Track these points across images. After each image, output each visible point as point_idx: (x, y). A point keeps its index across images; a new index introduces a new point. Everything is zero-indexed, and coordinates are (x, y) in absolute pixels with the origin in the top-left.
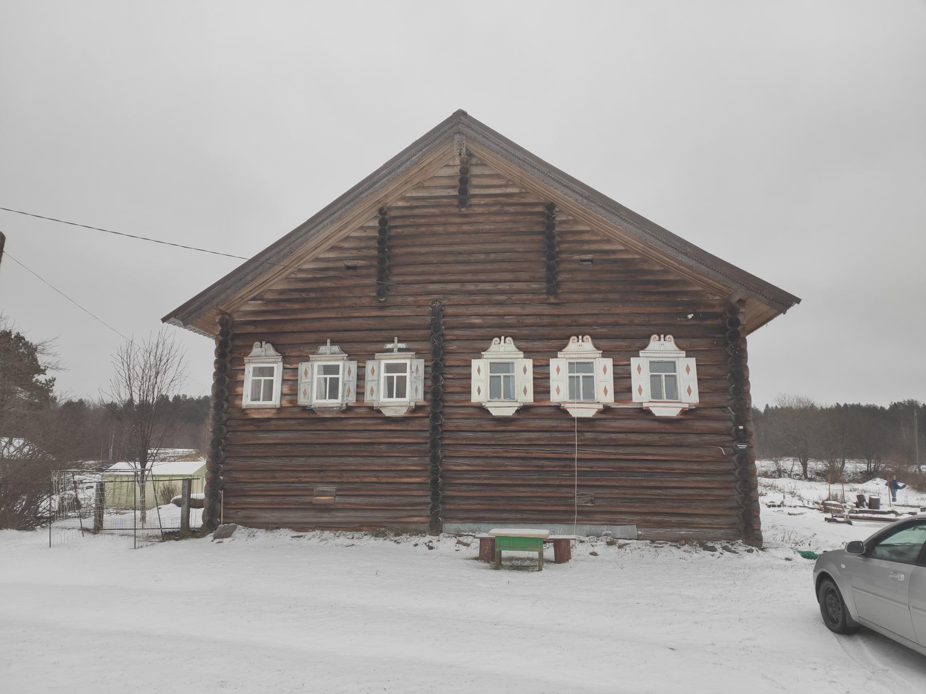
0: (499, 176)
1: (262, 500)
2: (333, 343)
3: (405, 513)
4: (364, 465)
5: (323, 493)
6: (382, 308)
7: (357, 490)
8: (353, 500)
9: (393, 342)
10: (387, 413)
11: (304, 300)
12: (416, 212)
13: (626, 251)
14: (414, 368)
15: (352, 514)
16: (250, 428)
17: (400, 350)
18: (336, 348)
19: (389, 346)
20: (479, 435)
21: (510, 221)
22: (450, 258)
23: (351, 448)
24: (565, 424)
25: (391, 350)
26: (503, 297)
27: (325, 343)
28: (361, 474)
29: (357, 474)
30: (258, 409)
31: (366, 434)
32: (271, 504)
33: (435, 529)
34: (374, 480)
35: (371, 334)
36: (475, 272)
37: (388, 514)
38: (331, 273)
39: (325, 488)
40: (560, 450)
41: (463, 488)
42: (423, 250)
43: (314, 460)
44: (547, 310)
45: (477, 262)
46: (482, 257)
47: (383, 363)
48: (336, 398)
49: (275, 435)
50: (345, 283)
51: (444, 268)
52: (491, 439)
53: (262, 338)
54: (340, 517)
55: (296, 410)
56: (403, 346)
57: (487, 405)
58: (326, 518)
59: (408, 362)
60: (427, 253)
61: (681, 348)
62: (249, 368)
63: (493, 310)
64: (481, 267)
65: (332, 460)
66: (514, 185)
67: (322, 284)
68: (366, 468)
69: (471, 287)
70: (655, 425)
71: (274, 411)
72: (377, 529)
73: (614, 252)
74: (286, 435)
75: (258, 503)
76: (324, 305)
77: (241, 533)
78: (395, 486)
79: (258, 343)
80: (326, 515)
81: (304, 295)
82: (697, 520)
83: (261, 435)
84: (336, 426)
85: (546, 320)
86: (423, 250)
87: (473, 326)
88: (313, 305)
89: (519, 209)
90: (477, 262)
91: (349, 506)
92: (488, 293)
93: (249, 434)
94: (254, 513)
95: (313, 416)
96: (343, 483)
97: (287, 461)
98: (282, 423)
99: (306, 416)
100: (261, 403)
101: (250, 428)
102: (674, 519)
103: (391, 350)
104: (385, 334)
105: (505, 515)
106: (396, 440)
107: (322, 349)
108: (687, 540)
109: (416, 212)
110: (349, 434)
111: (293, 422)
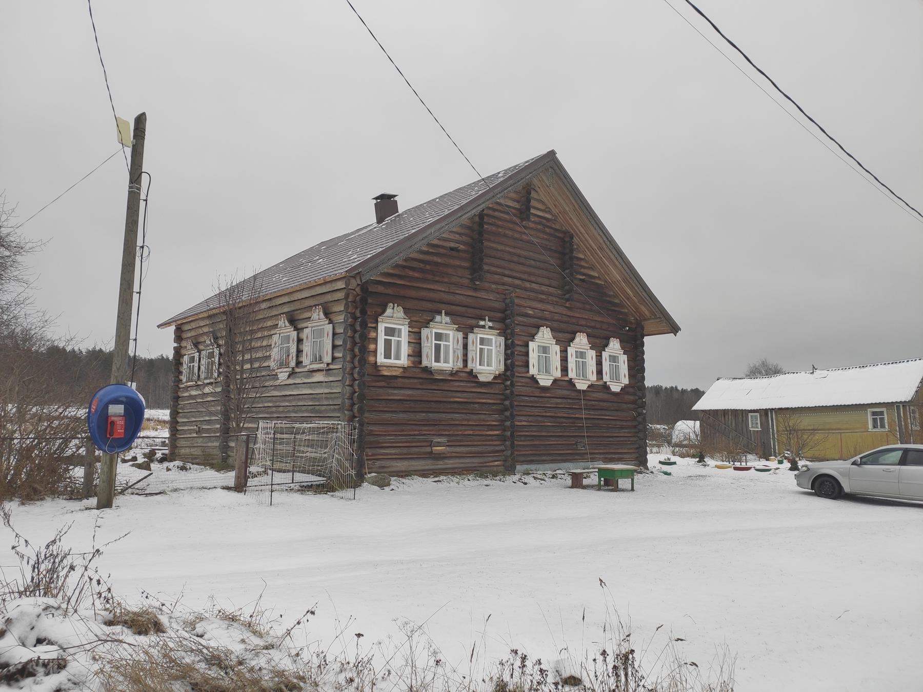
0: (543, 203)
1: (393, 451)
2: (446, 314)
3: (491, 459)
4: (466, 420)
5: (439, 444)
6: (476, 290)
7: (460, 441)
8: (458, 449)
9: (484, 320)
10: (482, 378)
11: (422, 271)
12: (496, 214)
13: (599, 278)
14: (498, 344)
15: (457, 461)
16: (383, 384)
17: (490, 328)
18: (448, 319)
19: (482, 323)
20: (532, 399)
21: (546, 239)
22: (515, 259)
23: (456, 406)
24: (574, 394)
25: (483, 327)
26: (544, 297)
27: (440, 313)
28: (464, 428)
29: (460, 428)
30: (389, 367)
31: (465, 395)
32: (401, 454)
33: (509, 470)
34: (471, 432)
35: (469, 310)
36: (530, 274)
37: (481, 460)
38: (441, 251)
39: (439, 440)
40: (571, 411)
41: (523, 438)
42: (500, 247)
43: (431, 415)
44: (565, 311)
45: (530, 266)
46: (533, 263)
47: (479, 336)
48: (448, 363)
49: (402, 392)
50: (452, 262)
51: (512, 266)
52: (536, 402)
53: (398, 299)
54: (450, 463)
55: (418, 370)
56: (490, 324)
57: (538, 377)
58: (440, 465)
59: (493, 338)
60: (502, 251)
61: (622, 348)
62: (381, 327)
63: (539, 305)
64: (533, 270)
65: (444, 416)
66: (550, 212)
67: (435, 259)
68: (466, 423)
69: (527, 285)
70: (574, 394)
71: (401, 370)
72: (481, 472)
73: (594, 277)
74: (409, 392)
75: (391, 454)
76: (437, 279)
77: (49, 499)
78: (483, 438)
79: (391, 304)
80: (441, 462)
81: (422, 265)
82: (625, 456)
83: (391, 391)
84: (445, 387)
85: (565, 319)
86: (500, 247)
87: (527, 315)
88: (430, 277)
89: (552, 231)
90: (530, 266)
91: (454, 454)
92: (536, 292)
93: (381, 390)
94: (388, 463)
95: (430, 377)
96: (453, 435)
97: (412, 416)
98: (407, 381)
99: (424, 376)
100: (392, 361)
101: (383, 384)
102: (616, 456)
103: (483, 327)
104: (478, 312)
105: (544, 458)
106: (484, 401)
107: (438, 318)
108: (436, 473)
109: (496, 214)
110: (455, 394)
111: (416, 381)
